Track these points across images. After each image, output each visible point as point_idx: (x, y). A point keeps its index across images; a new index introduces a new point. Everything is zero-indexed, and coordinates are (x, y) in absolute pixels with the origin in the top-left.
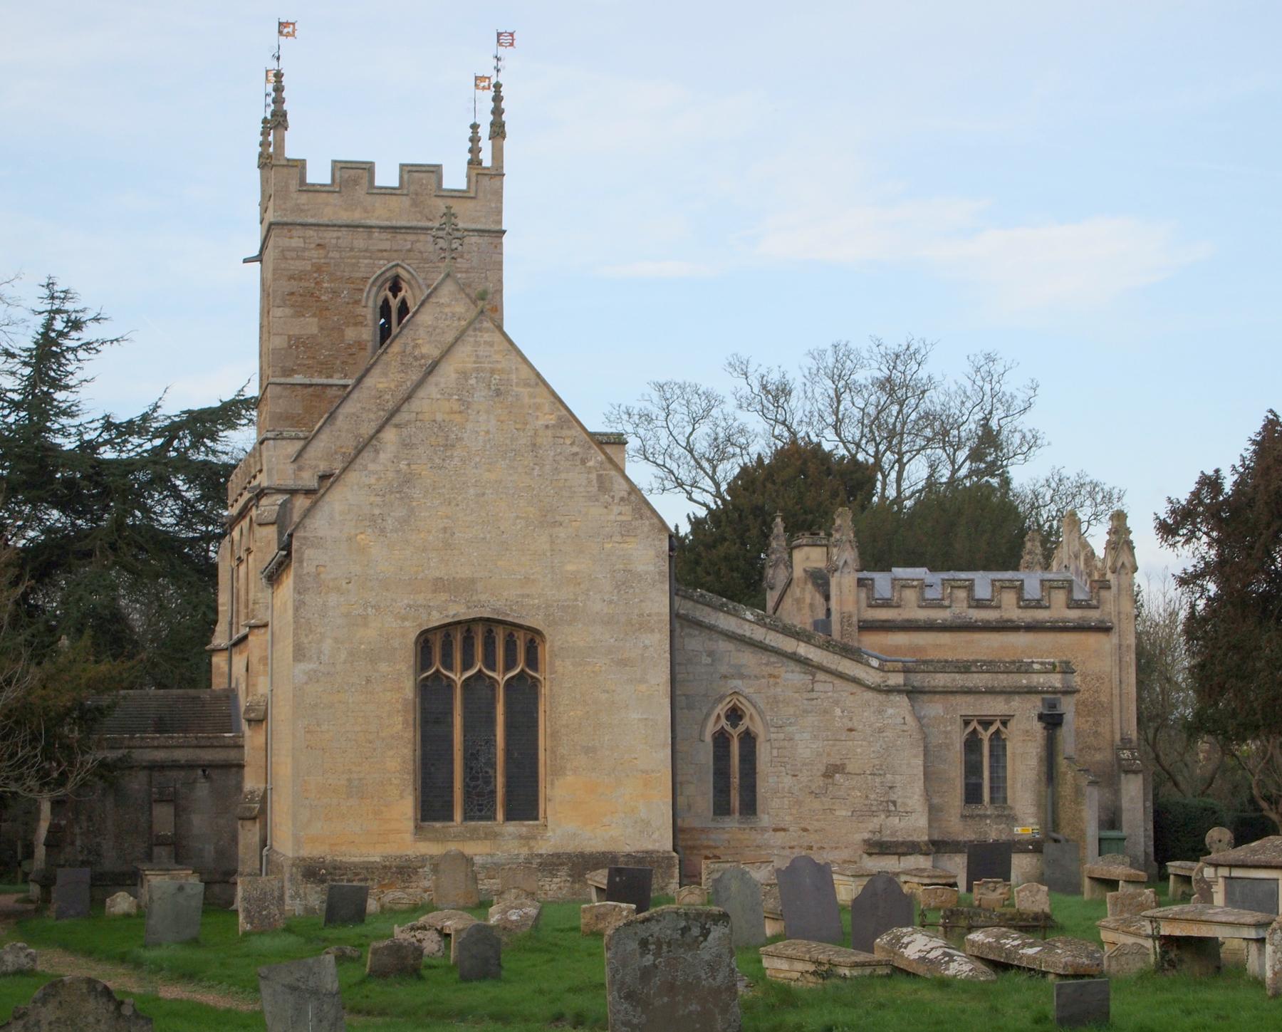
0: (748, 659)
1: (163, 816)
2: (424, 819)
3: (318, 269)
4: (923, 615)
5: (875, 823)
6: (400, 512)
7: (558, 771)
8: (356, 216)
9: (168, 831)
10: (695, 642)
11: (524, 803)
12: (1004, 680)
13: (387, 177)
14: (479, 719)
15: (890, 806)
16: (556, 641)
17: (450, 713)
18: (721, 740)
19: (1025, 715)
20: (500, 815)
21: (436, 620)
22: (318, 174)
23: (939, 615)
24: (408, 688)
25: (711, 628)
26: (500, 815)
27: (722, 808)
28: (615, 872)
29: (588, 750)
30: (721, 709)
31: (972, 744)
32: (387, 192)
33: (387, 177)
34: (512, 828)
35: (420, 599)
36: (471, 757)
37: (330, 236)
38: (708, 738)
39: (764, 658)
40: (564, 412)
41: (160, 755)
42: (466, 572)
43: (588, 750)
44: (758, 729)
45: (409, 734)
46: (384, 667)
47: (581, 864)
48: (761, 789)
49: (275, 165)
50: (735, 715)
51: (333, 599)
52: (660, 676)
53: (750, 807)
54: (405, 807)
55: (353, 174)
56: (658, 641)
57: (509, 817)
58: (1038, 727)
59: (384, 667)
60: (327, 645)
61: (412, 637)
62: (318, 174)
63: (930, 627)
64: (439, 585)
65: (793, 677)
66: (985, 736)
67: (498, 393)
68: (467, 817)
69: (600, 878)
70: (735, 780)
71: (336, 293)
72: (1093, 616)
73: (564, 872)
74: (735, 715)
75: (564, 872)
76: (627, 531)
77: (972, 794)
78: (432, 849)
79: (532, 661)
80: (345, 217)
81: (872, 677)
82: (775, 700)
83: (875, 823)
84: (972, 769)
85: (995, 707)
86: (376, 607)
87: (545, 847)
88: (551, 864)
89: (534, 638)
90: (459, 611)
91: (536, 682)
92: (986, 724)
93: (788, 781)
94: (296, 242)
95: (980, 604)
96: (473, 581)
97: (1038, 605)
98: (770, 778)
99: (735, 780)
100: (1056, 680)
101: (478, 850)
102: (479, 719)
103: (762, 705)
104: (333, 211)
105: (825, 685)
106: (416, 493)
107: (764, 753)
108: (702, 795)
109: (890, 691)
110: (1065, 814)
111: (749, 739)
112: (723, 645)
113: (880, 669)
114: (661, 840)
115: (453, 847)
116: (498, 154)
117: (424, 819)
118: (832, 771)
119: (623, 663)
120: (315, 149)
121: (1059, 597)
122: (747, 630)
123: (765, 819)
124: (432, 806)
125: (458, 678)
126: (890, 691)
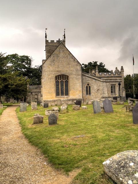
0: (89, 79)
1: (36, 96)
2: (57, 96)
3: (50, 49)
4: (104, 76)
5: (102, 95)
6: (53, 64)
7: (71, 90)
8: (53, 45)
9: (36, 98)
10: (84, 77)
11: (67, 94)
12: (115, 81)
13: (55, 41)
14: (62, 85)
15: (104, 93)
16: (70, 77)
17: (59, 85)
18: (87, 87)
19: (117, 84)
20: (60, 95)
21: (57, 75)
22: (49, 41)
23: (106, 76)
24: (54, 82)
25: (86, 76)
26: (60, 95)
27: (87, 94)
28: (77, 101)
29: (73, 88)
30: (87, 84)
31: (112, 87)
32: (55, 43)
33: (55, 41)
34: (66, 96)
35: (56, 73)
36: (61, 89)
37: (51, 47)
38: (86, 87)
39: (91, 79)
40: (66, 49)
41: (36, 91)
42: (60, 70)
43: (73, 88)
44: (90, 86)
45: (54, 87)
46: (52, 80)
47: (73, 100)
48: (91, 92)
49: (47, 41)
50: (88, 84)
51: (46, 73)
52: (81, 80)
53: (90, 94)
54: (54, 94)
55: (52, 41)
56: (80, 77)
57: (66, 95)
58: (118, 85)
59: (52, 80)
60: (46, 78)
61: (55, 77)
62: (49, 41)
63: (105, 77)
64: (57, 71)
65: (94, 81)
66: (113, 86)
67: (63, 51)
68: (61, 95)
69: (75, 101)
70: (88, 91)
71: (51, 52)
72: (120, 76)
73: (71, 101)
74: (88, 84)
75: (71, 101)
76: (77, 65)
77: (112, 92)
78: (57, 99)
79: (67, 79)
80: (52, 45)
81: (102, 80)
82: (92, 83)
83: (102, 95)
84: (112, 89)
85: (114, 83)
86: (51, 74)
87: (69, 98)
88: (70, 100)
89: (68, 77)
90: (59, 74)
91: (68, 81)
92: (113, 85)
93: (94, 91)
94: (48, 47)
95: (110, 75)
96: (61, 71)
97: (115, 75)
98: (92, 91)
99: (88, 91)
100: (120, 81)
101: (62, 99)
102: (62, 85)
103: (91, 83)
104: (51, 45)
105: (97, 81)
106: (55, 62)
107: (91, 89)
108: (85, 92)
109: (104, 82)
110: (121, 94)
111: (90, 87)
112: (87, 77)
113: (103, 80)
114: (81, 98)
115: (59, 99)
116: (65, 40)
117: (57, 96)
118: (98, 90)
119: (77, 79)
120: (49, 39)
121: (117, 74)
122: (89, 76)
123: (91, 95)
124: (57, 94)
125: (60, 81)
126: (104, 82)
